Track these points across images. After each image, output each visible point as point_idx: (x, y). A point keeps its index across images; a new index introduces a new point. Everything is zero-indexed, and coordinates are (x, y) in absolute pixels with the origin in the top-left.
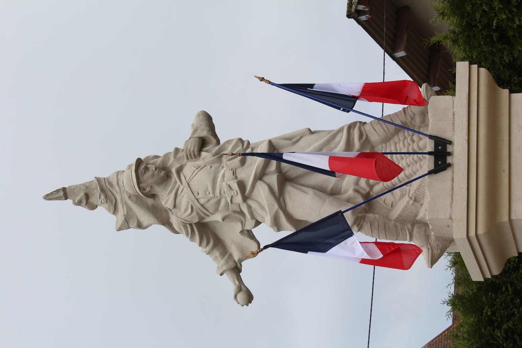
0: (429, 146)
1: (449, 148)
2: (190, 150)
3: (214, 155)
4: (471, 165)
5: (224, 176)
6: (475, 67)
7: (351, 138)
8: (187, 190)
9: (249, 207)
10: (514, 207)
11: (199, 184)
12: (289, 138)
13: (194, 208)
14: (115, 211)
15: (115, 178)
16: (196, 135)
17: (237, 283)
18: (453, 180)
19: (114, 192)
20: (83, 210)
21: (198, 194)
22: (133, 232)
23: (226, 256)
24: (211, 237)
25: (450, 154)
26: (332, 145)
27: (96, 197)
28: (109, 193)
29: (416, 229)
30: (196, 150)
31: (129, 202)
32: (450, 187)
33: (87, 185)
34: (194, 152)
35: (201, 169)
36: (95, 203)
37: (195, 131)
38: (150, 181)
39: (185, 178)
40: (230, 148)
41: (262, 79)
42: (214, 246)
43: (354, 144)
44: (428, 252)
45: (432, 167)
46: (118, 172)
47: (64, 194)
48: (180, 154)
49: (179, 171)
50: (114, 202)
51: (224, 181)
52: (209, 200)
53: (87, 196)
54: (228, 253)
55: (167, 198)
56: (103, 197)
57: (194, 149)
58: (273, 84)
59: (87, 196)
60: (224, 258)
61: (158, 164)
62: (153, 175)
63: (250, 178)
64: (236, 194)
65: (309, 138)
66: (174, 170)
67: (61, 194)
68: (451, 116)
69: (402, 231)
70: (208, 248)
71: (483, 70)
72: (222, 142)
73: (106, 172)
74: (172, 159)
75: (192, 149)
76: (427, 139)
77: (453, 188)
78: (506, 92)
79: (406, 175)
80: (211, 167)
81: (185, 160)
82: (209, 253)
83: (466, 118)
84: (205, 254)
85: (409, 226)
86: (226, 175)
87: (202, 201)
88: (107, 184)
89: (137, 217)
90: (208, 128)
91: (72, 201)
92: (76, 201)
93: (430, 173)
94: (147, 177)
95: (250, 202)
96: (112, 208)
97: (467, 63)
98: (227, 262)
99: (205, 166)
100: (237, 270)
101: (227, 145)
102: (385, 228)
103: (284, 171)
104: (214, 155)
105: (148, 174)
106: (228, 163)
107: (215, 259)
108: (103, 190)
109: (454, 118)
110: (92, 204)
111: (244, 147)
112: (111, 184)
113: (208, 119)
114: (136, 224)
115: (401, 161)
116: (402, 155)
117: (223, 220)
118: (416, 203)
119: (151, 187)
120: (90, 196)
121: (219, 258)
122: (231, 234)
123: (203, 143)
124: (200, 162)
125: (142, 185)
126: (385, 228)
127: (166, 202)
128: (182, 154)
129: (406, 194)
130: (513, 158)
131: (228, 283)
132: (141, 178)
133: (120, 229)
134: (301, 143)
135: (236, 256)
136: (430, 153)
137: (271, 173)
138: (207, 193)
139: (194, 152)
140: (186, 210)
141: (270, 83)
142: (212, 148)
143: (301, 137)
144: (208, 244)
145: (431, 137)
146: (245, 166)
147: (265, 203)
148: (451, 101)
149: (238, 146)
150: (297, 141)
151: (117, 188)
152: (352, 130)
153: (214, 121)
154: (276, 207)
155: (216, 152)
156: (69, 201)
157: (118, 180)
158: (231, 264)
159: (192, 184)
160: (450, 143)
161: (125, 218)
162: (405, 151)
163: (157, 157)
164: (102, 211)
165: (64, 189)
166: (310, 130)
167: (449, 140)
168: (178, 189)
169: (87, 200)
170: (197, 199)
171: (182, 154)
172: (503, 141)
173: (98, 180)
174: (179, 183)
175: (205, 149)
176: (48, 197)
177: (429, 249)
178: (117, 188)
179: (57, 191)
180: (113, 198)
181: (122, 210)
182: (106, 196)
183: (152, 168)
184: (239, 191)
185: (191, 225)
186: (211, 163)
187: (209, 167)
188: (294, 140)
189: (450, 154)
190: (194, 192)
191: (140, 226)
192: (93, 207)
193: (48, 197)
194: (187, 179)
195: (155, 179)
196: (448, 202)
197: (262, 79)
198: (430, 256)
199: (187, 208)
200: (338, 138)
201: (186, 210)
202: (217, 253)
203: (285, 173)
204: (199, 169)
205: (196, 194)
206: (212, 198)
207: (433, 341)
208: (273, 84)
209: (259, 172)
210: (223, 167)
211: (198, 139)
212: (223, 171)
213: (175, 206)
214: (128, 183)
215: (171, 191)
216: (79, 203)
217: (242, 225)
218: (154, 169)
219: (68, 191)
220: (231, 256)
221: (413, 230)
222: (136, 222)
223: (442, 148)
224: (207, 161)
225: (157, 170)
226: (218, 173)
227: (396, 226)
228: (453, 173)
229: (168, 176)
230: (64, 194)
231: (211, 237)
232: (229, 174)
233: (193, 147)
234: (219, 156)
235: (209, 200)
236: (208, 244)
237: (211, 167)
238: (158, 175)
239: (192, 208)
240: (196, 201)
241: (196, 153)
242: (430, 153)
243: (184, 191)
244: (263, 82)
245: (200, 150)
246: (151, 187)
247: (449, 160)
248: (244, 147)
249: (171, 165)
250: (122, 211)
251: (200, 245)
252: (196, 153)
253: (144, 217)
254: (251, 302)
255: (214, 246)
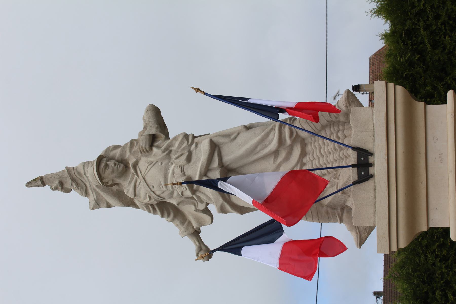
0: (353, 158)
1: (371, 160)
2: (142, 147)
3: (164, 152)
4: (391, 183)
5: (173, 172)
6: (391, 85)
7: (283, 136)
8: (143, 183)
9: (199, 197)
10: (431, 216)
11: (152, 174)
12: (226, 135)
13: (152, 197)
14: (86, 194)
15: (82, 169)
16: (146, 133)
17: (197, 244)
18: (375, 190)
19: (84, 181)
20: (59, 193)
21: (153, 187)
22: (103, 210)
23: (186, 224)
24: (171, 210)
25: (371, 165)
26: (266, 142)
27: (68, 183)
28: (79, 181)
29: (345, 214)
30: (147, 146)
31: (97, 190)
32: (373, 196)
33: (60, 175)
34: (146, 149)
35: (154, 165)
36: (69, 188)
37: (145, 128)
38: (111, 176)
39: (141, 173)
40: (177, 144)
41: (198, 90)
42: (175, 217)
43: (285, 140)
44: (357, 236)
45: (356, 178)
46: (85, 163)
47: (41, 181)
48: (135, 148)
49: (135, 165)
50: (85, 188)
51: (174, 177)
52: (163, 192)
53: (61, 184)
54: (187, 221)
55: (128, 189)
56: (74, 185)
57: (146, 146)
58: (208, 95)
59: (61, 184)
60: (184, 226)
61: (117, 156)
62: (113, 172)
63: (196, 174)
64: (185, 189)
65: (245, 135)
66: (131, 163)
67: (40, 183)
68: (371, 127)
69: (333, 217)
70: (170, 219)
71: (399, 88)
72: (171, 136)
73: (75, 163)
74: (128, 154)
75: (144, 147)
76: (350, 151)
77: (375, 197)
78: (421, 104)
79: (334, 159)
80: (162, 163)
81: (140, 154)
82: (172, 221)
83: (385, 151)
84: (195, 92)
85: (339, 210)
86: (175, 172)
87: (158, 193)
88: (76, 174)
89: (106, 200)
90: (156, 125)
91: (49, 187)
92: (53, 188)
93: (354, 183)
94: (108, 175)
95: (198, 194)
96: (84, 193)
97: (384, 82)
98: (187, 229)
99: (157, 162)
100: (196, 234)
101: (174, 142)
102: (318, 215)
103: (226, 165)
104: (164, 152)
105: (109, 171)
106: (175, 161)
107: (177, 225)
108: (73, 180)
109: (374, 129)
110: (67, 189)
111: (189, 143)
112: (79, 174)
113: (156, 112)
114: (105, 205)
115: (328, 156)
116: (328, 170)
117: (178, 204)
118: (344, 195)
119: (113, 180)
120: (64, 183)
121: (180, 226)
122: (188, 210)
123: (153, 139)
124: (152, 159)
125: (104, 181)
126: (318, 215)
127: (127, 192)
128: (136, 148)
129: (334, 185)
130: (430, 170)
131: (190, 245)
132: (102, 175)
133: (93, 209)
134: (239, 140)
135: (195, 226)
136: (353, 166)
137: (215, 169)
138: (161, 187)
139: (146, 149)
140: (145, 198)
141: (205, 93)
142: (162, 143)
143: (239, 134)
144: (169, 216)
145: (354, 149)
146: (191, 163)
147: (211, 197)
148: (371, 112)
149: (184, 143)
150: (235, 138)
151: (85, 177)
152: (283, 128)
153: (162, 114)
154: (221, 200)
155: (165, 149)
156: (47, 187)
157: (85, 172)
158: (191, 230)
159: (147, 178)
160: (372, 154)
161: (96, 202)
162: (330, 166)
163: (116, 147)
164: (74, 194)
165: (41, 178)
166: (245, 127)
167: (371, 152)
168: (136, 182)
169: (62, 186)
170: (153, 192)
171: (136, 148)
172: (420, 153)
173: (68, 169)
174: (135, 176)
175: (156, 144)
176: (29, 185)
177: (357, 233)
178: (85, 177)
179: (35, 180)
180: (83, 185)
181: (92, 195)
182: (77, 184)
183: (111, 163)
184: (187, 188)
185: (152, 205)
186: (163, 159)
187: (160, 164)
188: (232, 137)
189: (371, 165)
190: (149, 185)
191: (109, 206)
192: (68, 191)
193: (29, 185)
194: (143, 174)
195: (115, 174)
196: (372, 211)
197: (198, 90)
198: (359, 240)
199: (146, 197)
200: (271, 136)
201: (145, 198)
202: (178, 222)
203: (227, 166)
204: (152, 165)
205: (151, 187)
206: (165, 191)
207: (377, 52)
208: (208, 95)
209: (203, 170)
210: (172, 164)
211: (148, 137)
212: (172, 167)
213: (135, 195)
214: (91, 176)
215: (131, 182)
216: (56, 189)
217: (195, 206)
218: (113, 165)
219: (44, 180)
220: (190, 223)
221: (342, 215)
222: (106, 204)
223: (364, 159)
224: (158, 158)
225: (116, 166)
226: (169, 169)
227: (327, 212)
228: (375, 183)
229: (126, 166)
230: (41, 181)
231: (171, 210)
232: (178, 171)
233: (144, 143)
234: (168, 152)
235: (163, 192)
236: (169, 216)
237: (162, 163)
238: (117, 170)
239: (150, 198)
240: (152, 193)
241: (148, 149)
242: (353, 166)
243: (141, 184)
244: (199, 93)
245: (151, 146)
246: (113, 180)
247: (371, 171)
248: (189, 143)
249: (128, 158)
250: (92, 196)
251: (162, 216)
252: (148, 149)
253: (111, 201)
254: (211, 258)
255: (175, 217)
